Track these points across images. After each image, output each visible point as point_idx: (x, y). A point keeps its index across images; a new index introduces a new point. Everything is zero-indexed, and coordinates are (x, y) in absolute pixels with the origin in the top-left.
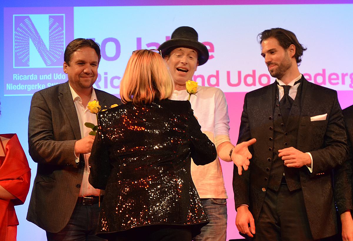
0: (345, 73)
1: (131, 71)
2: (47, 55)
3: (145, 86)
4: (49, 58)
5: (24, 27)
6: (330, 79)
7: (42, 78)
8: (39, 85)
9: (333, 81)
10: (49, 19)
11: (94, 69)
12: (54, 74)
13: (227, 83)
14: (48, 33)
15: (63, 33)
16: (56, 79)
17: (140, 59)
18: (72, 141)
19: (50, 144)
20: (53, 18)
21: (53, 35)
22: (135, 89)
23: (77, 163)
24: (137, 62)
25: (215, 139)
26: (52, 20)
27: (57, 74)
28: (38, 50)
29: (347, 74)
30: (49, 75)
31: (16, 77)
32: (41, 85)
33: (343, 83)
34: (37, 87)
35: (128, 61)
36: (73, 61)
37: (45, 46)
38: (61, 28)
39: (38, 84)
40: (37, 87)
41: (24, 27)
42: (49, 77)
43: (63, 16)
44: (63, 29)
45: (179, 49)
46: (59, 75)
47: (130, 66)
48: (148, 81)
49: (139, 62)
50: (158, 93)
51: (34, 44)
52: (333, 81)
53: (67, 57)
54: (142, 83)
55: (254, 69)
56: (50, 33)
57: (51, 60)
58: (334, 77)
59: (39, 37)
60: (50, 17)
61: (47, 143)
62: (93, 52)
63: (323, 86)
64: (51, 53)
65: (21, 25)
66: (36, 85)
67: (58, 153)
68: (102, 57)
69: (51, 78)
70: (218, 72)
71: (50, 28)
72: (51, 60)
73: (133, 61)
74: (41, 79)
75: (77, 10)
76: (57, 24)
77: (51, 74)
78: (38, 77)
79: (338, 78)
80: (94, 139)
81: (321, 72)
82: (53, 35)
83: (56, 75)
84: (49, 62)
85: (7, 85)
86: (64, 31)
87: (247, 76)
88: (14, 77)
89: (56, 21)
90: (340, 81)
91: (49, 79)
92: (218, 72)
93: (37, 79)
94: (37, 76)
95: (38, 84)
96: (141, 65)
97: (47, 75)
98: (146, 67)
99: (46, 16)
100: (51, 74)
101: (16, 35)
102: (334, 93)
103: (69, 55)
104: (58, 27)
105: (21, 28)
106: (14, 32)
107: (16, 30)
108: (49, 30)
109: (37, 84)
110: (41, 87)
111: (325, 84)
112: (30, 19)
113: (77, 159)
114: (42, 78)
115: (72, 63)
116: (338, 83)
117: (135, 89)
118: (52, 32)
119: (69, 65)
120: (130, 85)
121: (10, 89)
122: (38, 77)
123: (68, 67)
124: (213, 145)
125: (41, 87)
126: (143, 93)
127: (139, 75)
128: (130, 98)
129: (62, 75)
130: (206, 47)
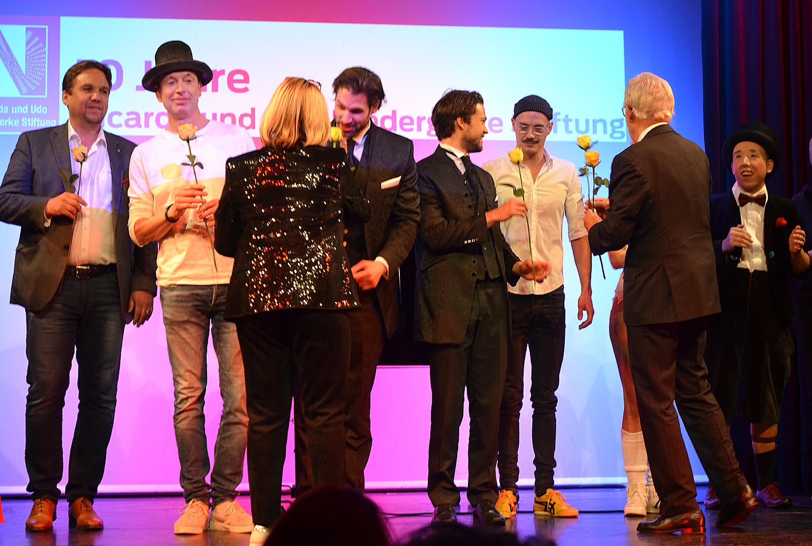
0: (421, 116)
1: (277, 104)
2: (22, 80)
3: (289, 123)
4: (25, 84)
6: (402, 124)
7: (14, 110)
8: (11, 120)
9: (406, 127)
10: (27, 31)
11: (103, 97)
12: (32, 106)
13: (612, 119)
14: (25, 51)
15: (45, 52)
16: (35, 112)
17: (291, 88)
18: (43, 199)
19: (9, 197)
20: (31, 30)
22: (278, 126)
23: (46, 227)
24: (286, 92)
26: (30, 33)
27: (35, 106)
28: (10, 74)
29: (424, 118)
30: (24, 108)
32: (12, 120)
33: (419, 129)
34: (8, 123)
35: (277, 88)
36: (76, 88)
37: (20, 68)
38: (42, 45)
39: (10, 119)
40: (8, 123)
42: (25, 110)
43: (45, 29)
45: (169, 76)
46: (38, 108)
47: (277, 95)
48: (294, 118)
49: (288, 93)
50: (303, 136)
51: (5, 65)
52: (406, 127)
53: (68, 84)
54: (287, 121)
55: (253, 107)
57: (28, 88)
58: (132, 123)
59: (12, 55)
60: (27, 29)
61: (15, 196)
62: (102, 76)
63: (392, 131)
64: (28, 77)
66: (6, 121)
67: (24, 210)
68: (211, 82)
69: (27, 111)
70: (253, 110)
71: (27, 44)
72: (28, 88)
73: (282, 89)
74: (13, 112)
75: (65, 21)
76: (37, 39)
77: (27, 106)
78: (10, 110)
79: (412, 123)
81: (249, 112)
83: (14, 109)
84: (24, 90)
86: (47, 49)
87: (243, 116)
89: (35, 35)
90: (415, 127)
91: (24, 112)
92: (253, 110)
93: (7, 111)
94: (7, 108)
95: (10, 119)
96: (290, 96)
97: (22, 107)
98: (296, 101)
99: (23, 28)
100: (27, 106)
102: (408, 143)
103: (71, 80)
104: (38, 43)
108: (26, 46)
109: (8, 119)
110: (13, 122)
111: (396, 130)
113: (47, 221)
114: (14, 110)
115: (76, 90)
116: (412, 130)
117: (278, 126)
118: (30, 49)
119: (71, 94)
120: (273, 120)
122: (10, 110)
123: (69, 97)
125: (13, 122)
126: (286, 133)
127: (285, 109)
128: (270, 137)
129: (42, 107)
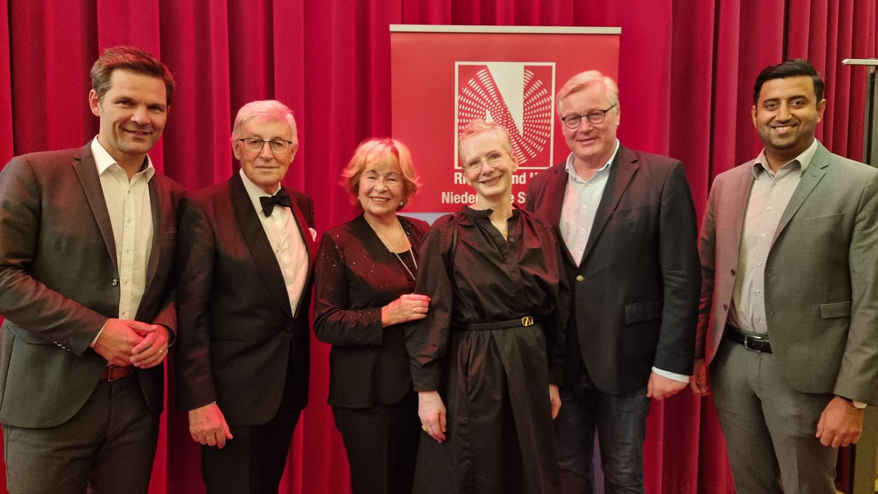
5: (477, 88)
21: (536, 135)
25: (503, 267)
26: (531, 74)
31: (460, 178)
41: (477, 88)
44: (549, 94)
56: (526, 101)
60: (526, 68)
65: (471, 82)
71: (526, 90)
76: (539, 83)
80: (162, 101)
82: (536, 135)
85: (444, 194)
88: (456, 178)
91: (521, 183)
101: (460, 102)
105: (471, 89)
106: (457, 98)
107: (461, 93)
112: (487, 70)
121: (448, 202)
124: (314, 233)
130: (811, 144)
